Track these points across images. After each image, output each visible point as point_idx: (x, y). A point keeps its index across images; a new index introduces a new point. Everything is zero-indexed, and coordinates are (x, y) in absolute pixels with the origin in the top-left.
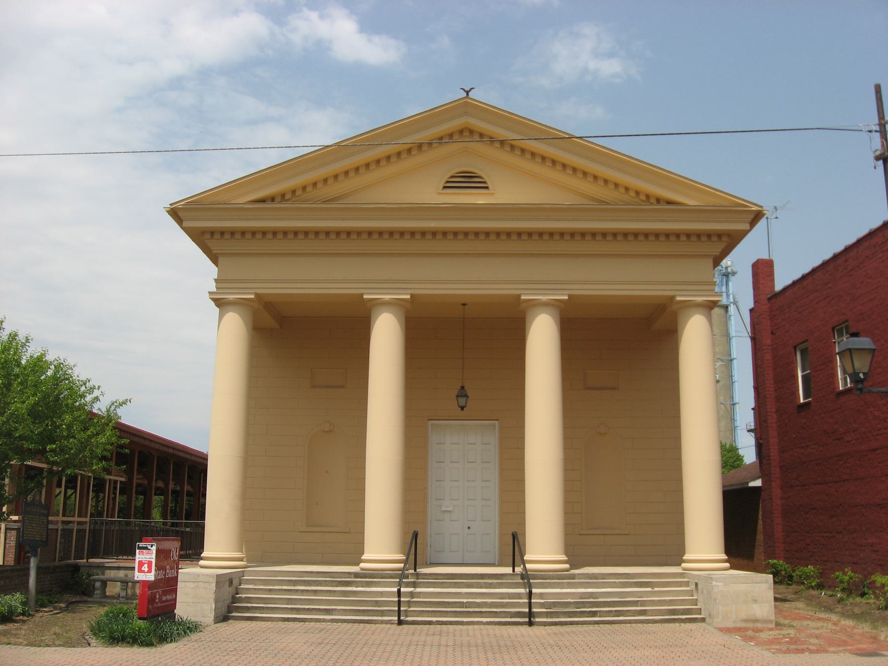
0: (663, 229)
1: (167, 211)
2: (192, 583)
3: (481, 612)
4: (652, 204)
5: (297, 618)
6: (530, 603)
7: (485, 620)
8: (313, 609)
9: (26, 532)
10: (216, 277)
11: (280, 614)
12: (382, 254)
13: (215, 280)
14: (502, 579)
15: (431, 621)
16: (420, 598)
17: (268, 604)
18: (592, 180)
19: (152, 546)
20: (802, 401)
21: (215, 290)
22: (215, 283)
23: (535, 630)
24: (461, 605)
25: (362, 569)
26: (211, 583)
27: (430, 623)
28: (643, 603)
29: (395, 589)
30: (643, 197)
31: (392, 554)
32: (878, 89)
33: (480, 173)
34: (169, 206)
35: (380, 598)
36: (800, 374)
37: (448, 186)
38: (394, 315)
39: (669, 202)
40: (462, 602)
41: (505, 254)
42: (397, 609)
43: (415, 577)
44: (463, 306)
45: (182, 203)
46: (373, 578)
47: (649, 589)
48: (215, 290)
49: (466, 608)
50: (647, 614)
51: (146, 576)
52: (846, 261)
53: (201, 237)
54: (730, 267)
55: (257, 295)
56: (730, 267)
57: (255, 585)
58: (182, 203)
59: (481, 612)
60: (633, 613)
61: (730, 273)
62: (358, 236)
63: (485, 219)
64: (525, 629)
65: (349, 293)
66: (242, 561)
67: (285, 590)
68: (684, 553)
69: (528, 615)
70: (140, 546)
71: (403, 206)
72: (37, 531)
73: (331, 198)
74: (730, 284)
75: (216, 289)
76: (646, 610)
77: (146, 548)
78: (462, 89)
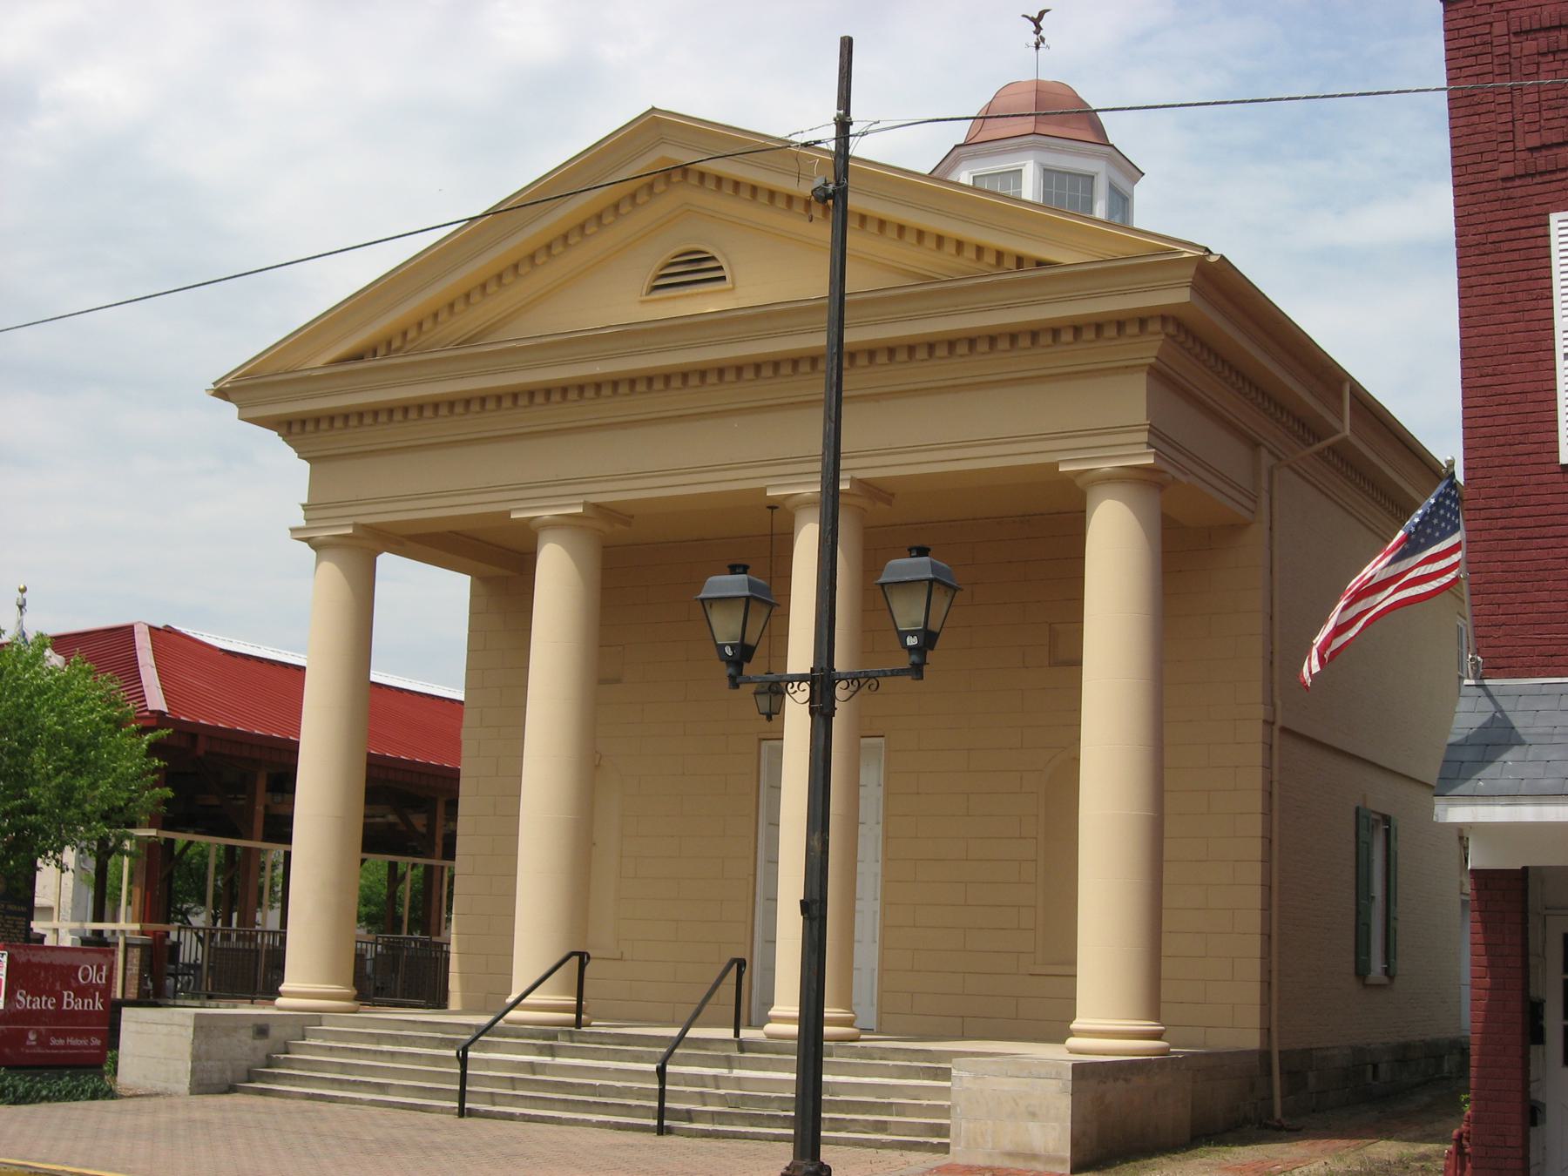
0: (322, 410)
1: (213, 395)
2: (164, 1026)
3: (606, 1104)
4: (1009, 271)
5: (324, 1095)
6: (662, 1091)
8: (361, 1082)
10: (305, 501)
11: (318, 1088)
12: (1098, 370)
13: (303, 505)
14: (708, 1050)
15: (513, 1113)
16: (545, 1074)
17: (316, 1071)
21: (303, 523)
22: (303, 512)
24: (593, 1090)
25: (770, 1036)
26: (188, 1026)
27: (510, 1117)
28: (886, 1108)
29: (653, 1067)
30: (990, 259)
31: (836, 1007)
32: (847, 45)
33: (712, 252)
34: (213, 387)
35: (484, 1070)
37: (664, 282)
38: (563, 547)
39: (1040, 264)
40: (592, 1085)
41: (916, 390)
42: (458, 1087)
43: (568, 1038)
44: (770, 511)
45: (229, 379)
46: (504, 1037)
48: (303, 523)
49: (600, 1096)
50: (889, 1131)
53: (290, 428)
55: (356, 526)
57: (325, 1040)
58: (227, 380)
59: (606, 1104)
60: (865, 1127)
62: (1119, 331)
63: (1154, 289)
64: (653, 1138)
65: (940, 470)
66: (851, 1026)
67: (352, 1049)
68: (1072, 1016)
69: (666, 1114)
71: (544, 340)
75: (305, 521)
76: (885, 1122)
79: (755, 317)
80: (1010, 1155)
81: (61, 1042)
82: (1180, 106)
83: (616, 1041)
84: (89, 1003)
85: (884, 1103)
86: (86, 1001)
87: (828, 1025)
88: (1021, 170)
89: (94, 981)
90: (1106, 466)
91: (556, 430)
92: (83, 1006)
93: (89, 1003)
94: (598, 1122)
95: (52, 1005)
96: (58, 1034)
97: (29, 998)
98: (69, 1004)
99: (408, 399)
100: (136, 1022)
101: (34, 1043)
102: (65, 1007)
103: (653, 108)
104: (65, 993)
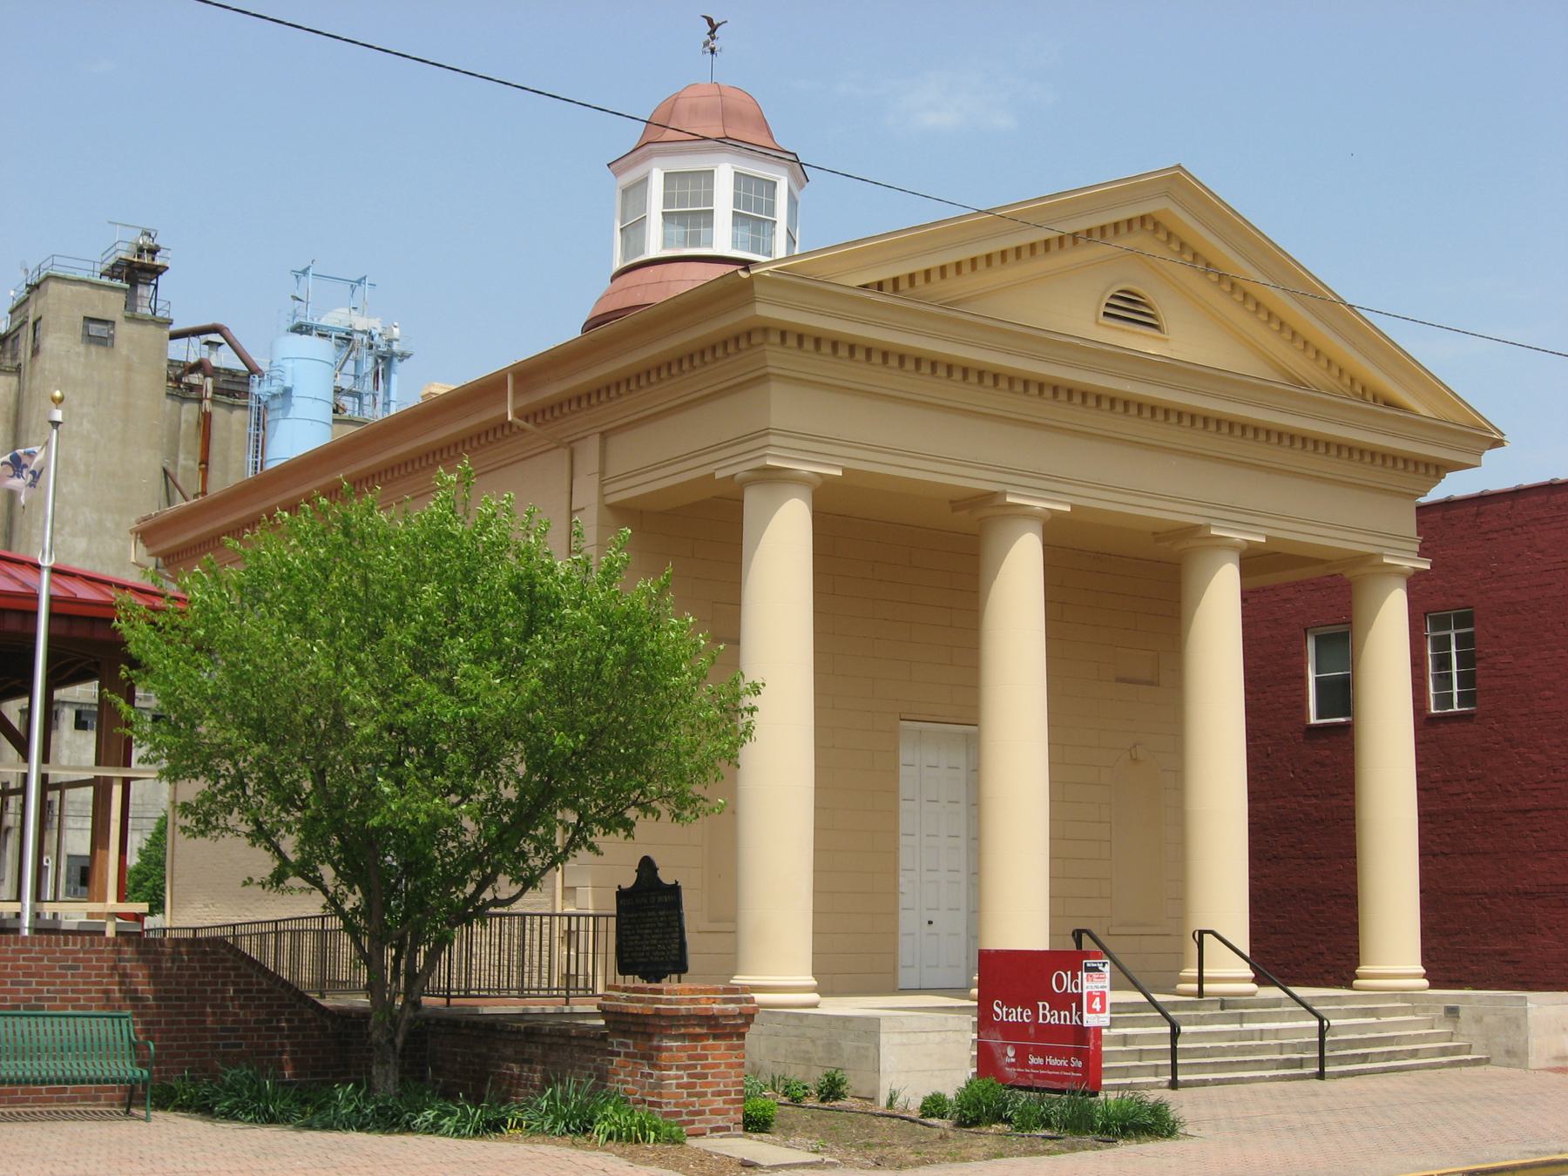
2: (936, 1034)
7: (1267, 1074)
9: (628, 949)
14: (1198, 1010)
18: (1301, 346)
19: (1104, 964)
20: (1313, 720)
23: (1327, 1084)
27: (1204, 1083)
36: (1311, 676)
39: (1389, 404)
42: (1169, 1062)
45: (770, 268)
47: (1373, 1020)
51: (1099, 1018)
52: (1478, 515)
54: (397, 340)
55: (844, 470)
56: (397, 340)
59: (1245, 1062)
61: (397, 356)
68: (1358, 965)
70: (1089, 965)
72: (655, 942)
73: (954, 299)
74: (394, 378)
76: (1417, 1050)
77: (1096, 969)
78: (704, 17)
79: (1096, 352)
80: (1556, 1058)
81: (1040, 1061)
82: (254, 15)
83: (1132, 1009)
84: (1065, 1015)
85: (1421, 1035)
86: (1062, 1013)
87: (1194, 977)
88: (713, 171)
89: (1069, 991)
90: (806, 468)
91: (1228, 459)
92: (1059, 1020)
93: (1065, 1015)
94: (1270, 1077)
95: (1028, 1017)
96: (1040, 1052)
97: (1005, 1009)
98: (1045, 1017)
99: (1419, 455)
100: (901, 1033)
101: (1013, 1060)
102: (1041, 1021)
103: (1179, 167)
104: (1040, 1004)
